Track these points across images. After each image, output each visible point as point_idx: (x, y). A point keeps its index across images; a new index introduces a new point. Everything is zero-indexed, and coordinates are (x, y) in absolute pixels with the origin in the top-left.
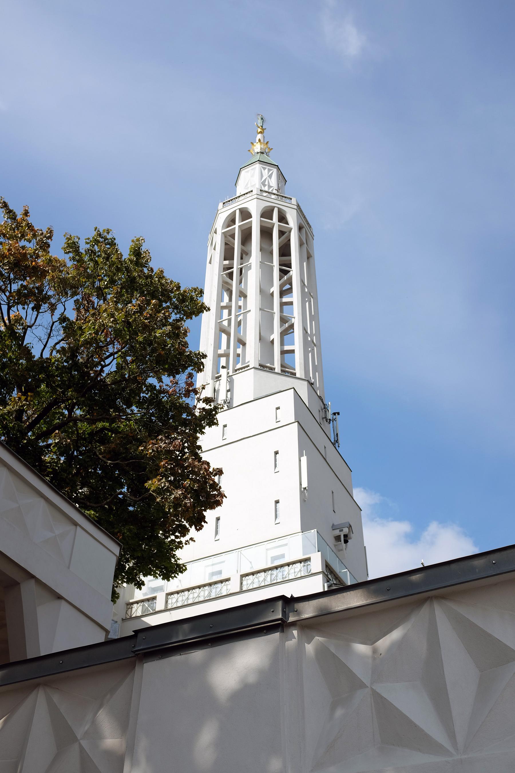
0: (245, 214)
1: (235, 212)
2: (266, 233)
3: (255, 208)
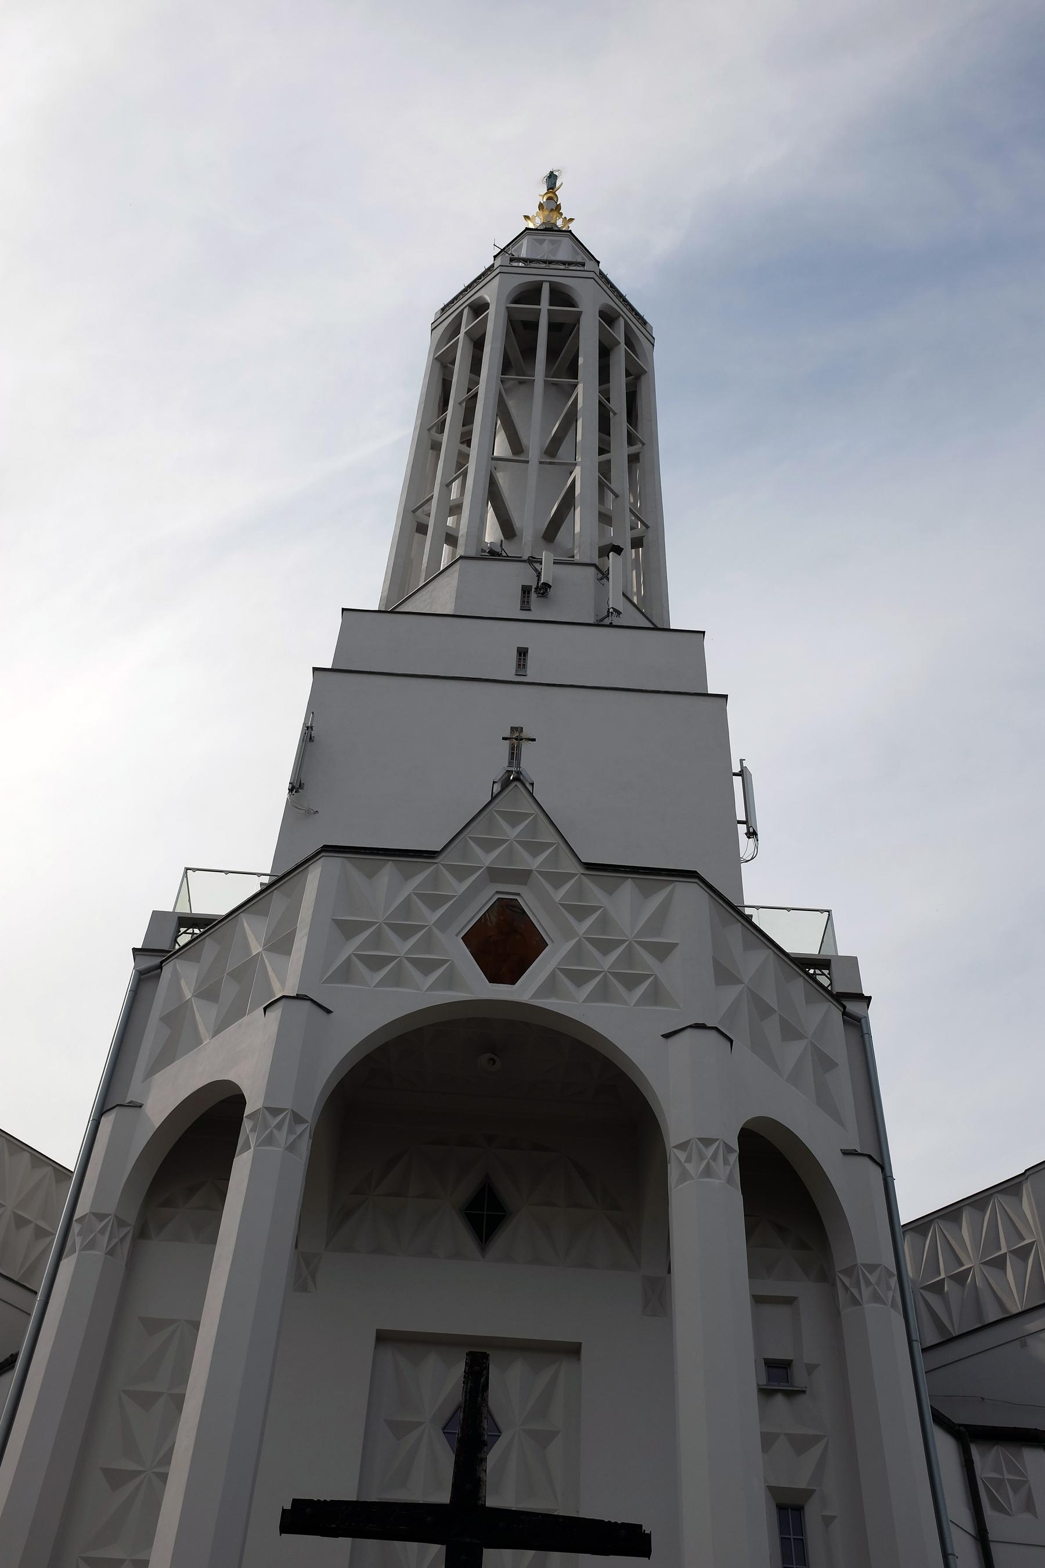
0: (479, 308)
1: (462, 312)
2: (521, 330)
3: (489, 294)
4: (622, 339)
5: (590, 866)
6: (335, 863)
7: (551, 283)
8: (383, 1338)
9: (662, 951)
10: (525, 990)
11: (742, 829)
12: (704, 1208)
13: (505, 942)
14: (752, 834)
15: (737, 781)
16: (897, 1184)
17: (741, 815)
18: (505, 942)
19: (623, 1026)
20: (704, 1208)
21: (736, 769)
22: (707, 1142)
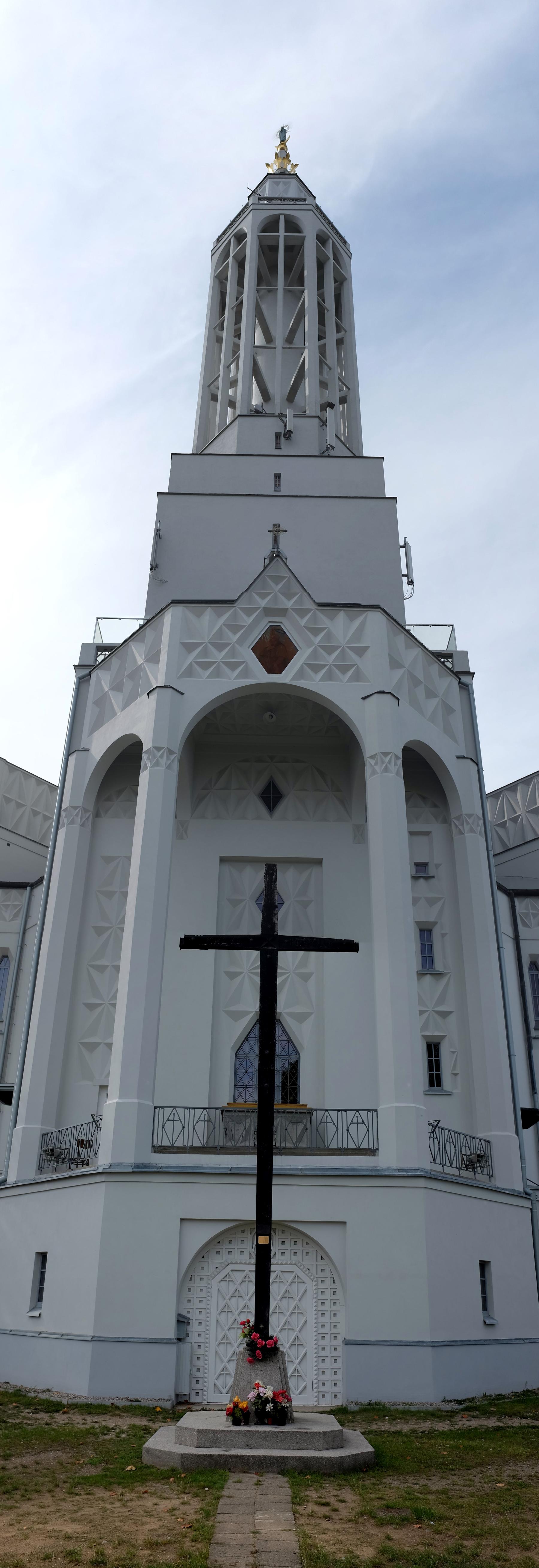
0: (240, 237)
1: (229, 242)
3: (247, 226)
4: (331, 255)
5: (320, 605)
6: (178, 610)
7: (285, 215)
8: (223, 860)
9: (361, 651)
10: (287, 677)
11: (405, 579)
12: (384, 787)
13: (275, 650)
14: (410, 582)
15: (402, 550)
16: (334, 224)
17: (404, 572)
18: (275, 650)
19: (341, 695)
20: (384, 787)
21: (402, 543)
22: (386, 754)
